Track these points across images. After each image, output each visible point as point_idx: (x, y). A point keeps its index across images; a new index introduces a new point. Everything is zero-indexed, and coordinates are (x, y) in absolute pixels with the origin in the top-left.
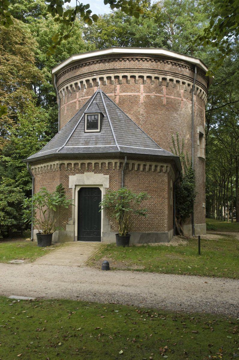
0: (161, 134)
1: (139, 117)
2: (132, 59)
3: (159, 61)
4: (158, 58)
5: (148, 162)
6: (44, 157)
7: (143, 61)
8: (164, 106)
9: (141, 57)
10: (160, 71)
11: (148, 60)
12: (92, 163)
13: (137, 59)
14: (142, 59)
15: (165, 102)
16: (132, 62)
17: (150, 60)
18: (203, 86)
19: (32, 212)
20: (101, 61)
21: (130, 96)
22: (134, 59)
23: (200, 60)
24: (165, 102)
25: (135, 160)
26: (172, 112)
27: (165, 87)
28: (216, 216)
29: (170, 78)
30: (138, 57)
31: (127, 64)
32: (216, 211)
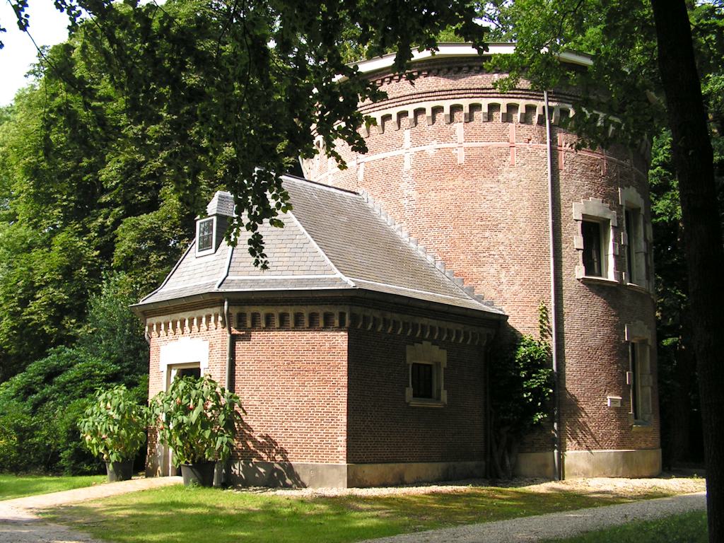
0: (455, 235)
1: (402, 202)
4: (434, 64)
5: (290, 307)
6: (464, 311)
8: (460, 167)
10: (443, 93)
12: (288, 315)
15: (461, 159)
21: (384, 159)
24: (461, 159)
25: (258, 305)
26: (481, 179)
27: (462, 123)
28: (179, 534)
29: (451, 104)
32: (522, 503)
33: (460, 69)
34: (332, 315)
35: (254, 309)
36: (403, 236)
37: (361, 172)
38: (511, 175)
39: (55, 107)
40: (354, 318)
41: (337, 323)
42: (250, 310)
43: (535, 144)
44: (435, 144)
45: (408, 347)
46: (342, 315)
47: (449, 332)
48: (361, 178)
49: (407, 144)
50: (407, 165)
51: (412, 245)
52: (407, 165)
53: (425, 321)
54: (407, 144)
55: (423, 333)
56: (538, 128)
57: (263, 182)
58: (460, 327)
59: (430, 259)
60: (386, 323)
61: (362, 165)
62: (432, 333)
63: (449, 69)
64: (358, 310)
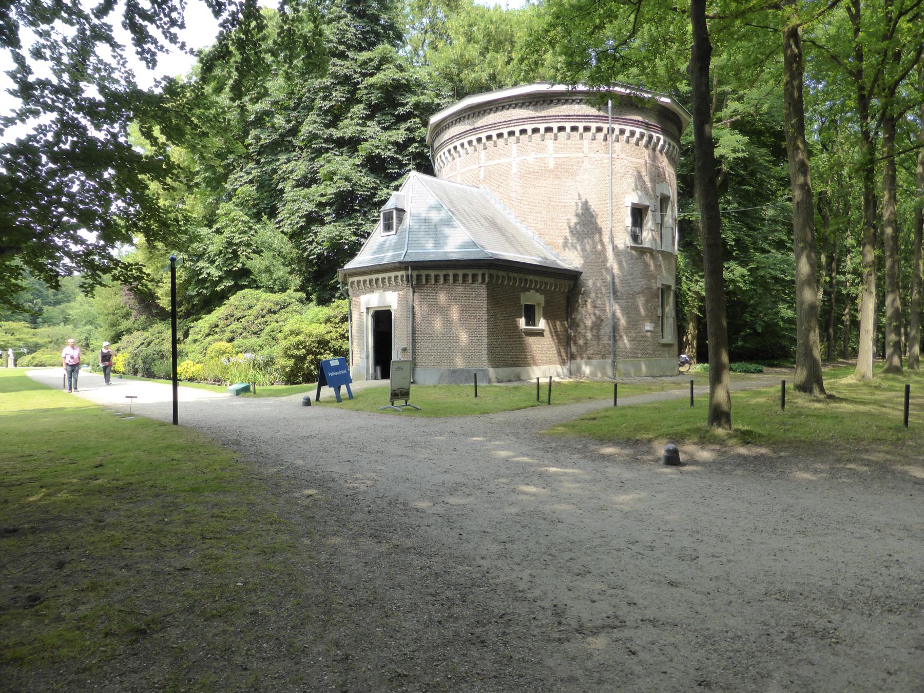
1: (512, 194)
8: (551, 171)
15: (551, 165)
24: (551, 165)
33: (552, 101)
34: (477, 275)
35: (427, 272)
36: (512, 218)
37: (482, 173)
38: (586, 176)
39: (310, 32)
40: (491, 276)
41: (480, 280)
42: (424, 273)
43: (602, 154)
44: (533, 155)
45: (522, 294)
46: (483, 275)
47: (536, 282)
48: (482, 177)
49: (514, 154)
50: (514, 169)
51: (518, 225)
52: (514, 169)
53: (531, 277)
54: (514, 154)
55: (531, 285)
56: (604, 143)
57: (20, 174)
58: (552, 280)
59: (530, 234)
60: (509, 278)
61: (482, 169)
62: (536, 285)
63: (544, 102)
64: (494, 272)
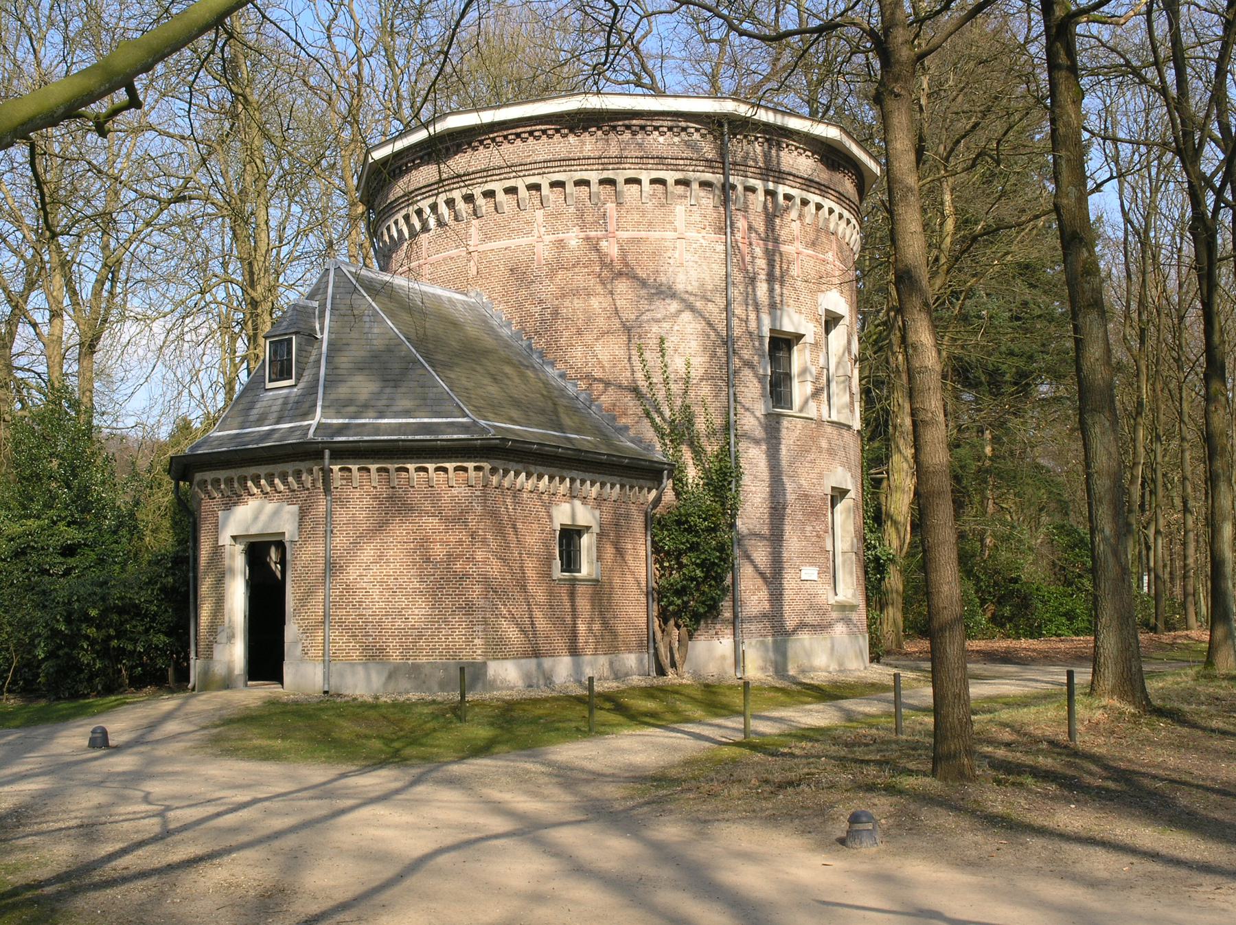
2: (505, 137)
3: (585, 129)
7: (537, 138)
9: (528, 129)
11: (550, 132)
13: (518, 135)
14: (531, 133)
16: (506, 146)
17: (557, 131)
18: (841, 198)
19: (743, 183)
20: (421, 158)
22: (550, 132)
23: (843, 129)
30: (519, 130)
31: (512, 151)
